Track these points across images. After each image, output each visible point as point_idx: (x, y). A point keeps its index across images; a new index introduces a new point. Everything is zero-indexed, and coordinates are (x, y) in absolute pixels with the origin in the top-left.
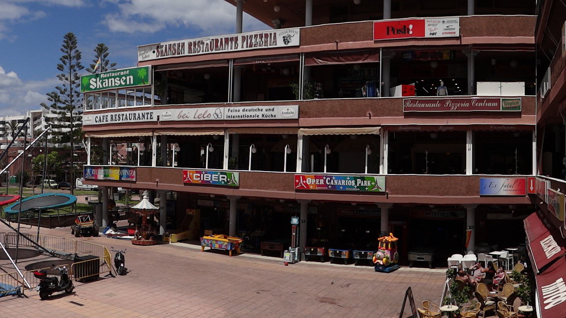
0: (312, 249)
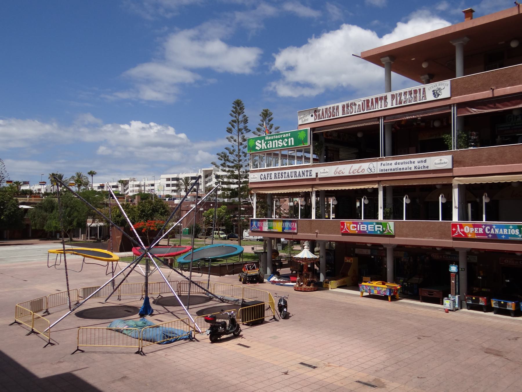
0: (474, 298)
